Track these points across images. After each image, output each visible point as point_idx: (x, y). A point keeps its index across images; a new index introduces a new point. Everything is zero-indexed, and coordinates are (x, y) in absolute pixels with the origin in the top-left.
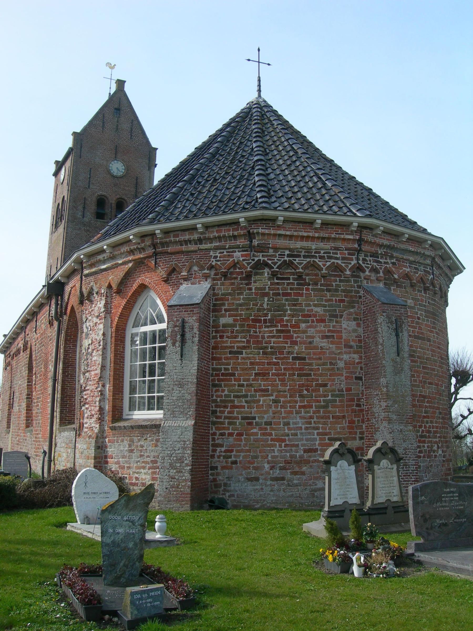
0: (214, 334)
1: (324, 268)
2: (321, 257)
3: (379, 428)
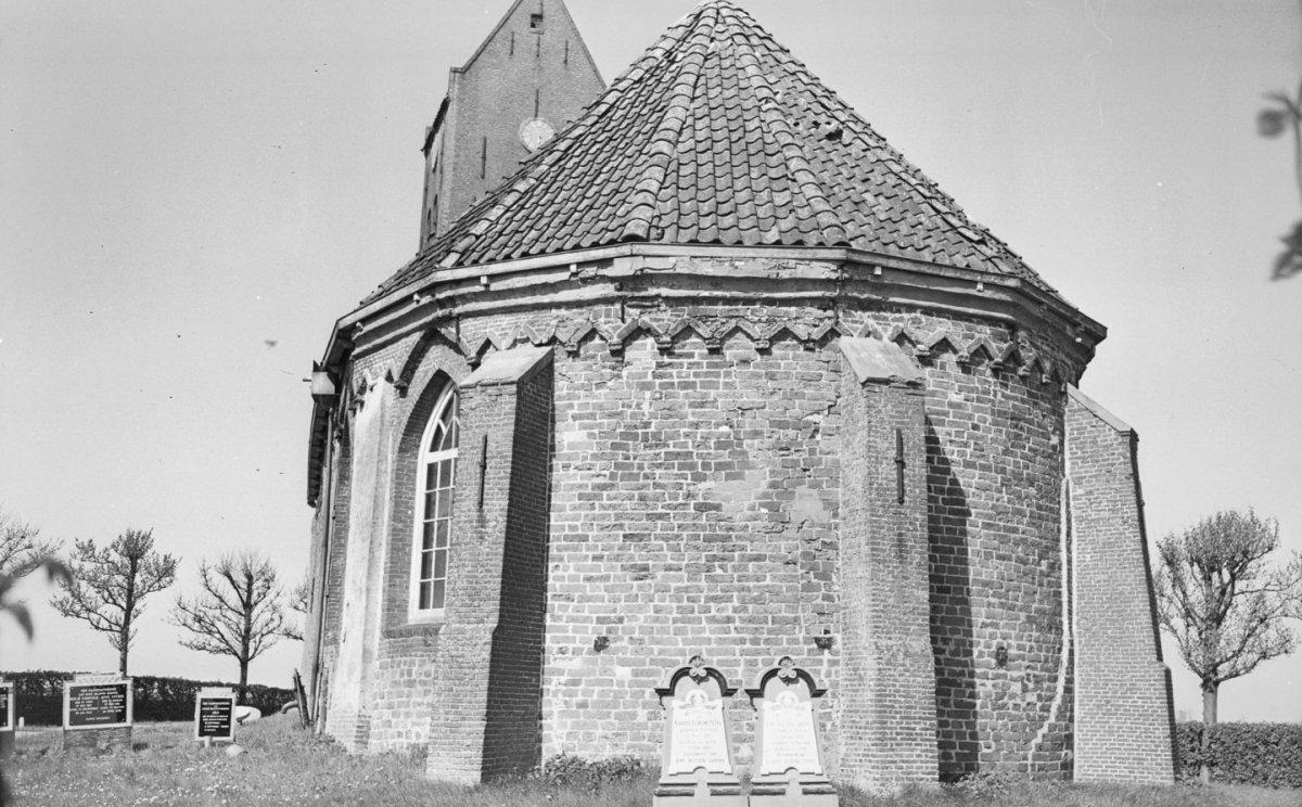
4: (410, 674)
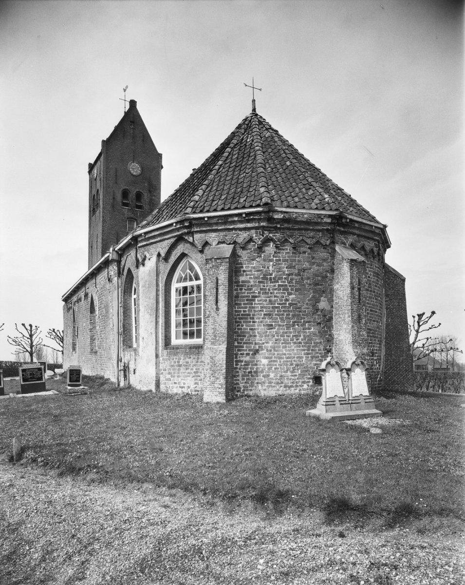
0: (236, 288)
4: (178, 362)
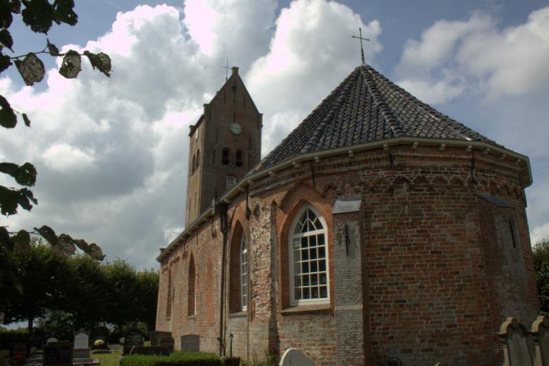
1: (449, 181)
2: (446, 173)
3: (504, 306)
